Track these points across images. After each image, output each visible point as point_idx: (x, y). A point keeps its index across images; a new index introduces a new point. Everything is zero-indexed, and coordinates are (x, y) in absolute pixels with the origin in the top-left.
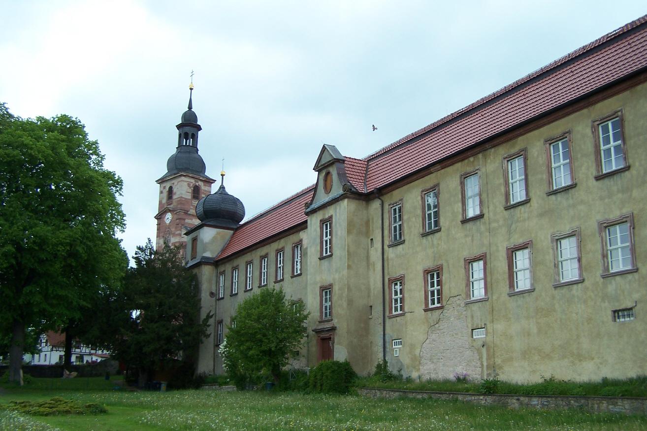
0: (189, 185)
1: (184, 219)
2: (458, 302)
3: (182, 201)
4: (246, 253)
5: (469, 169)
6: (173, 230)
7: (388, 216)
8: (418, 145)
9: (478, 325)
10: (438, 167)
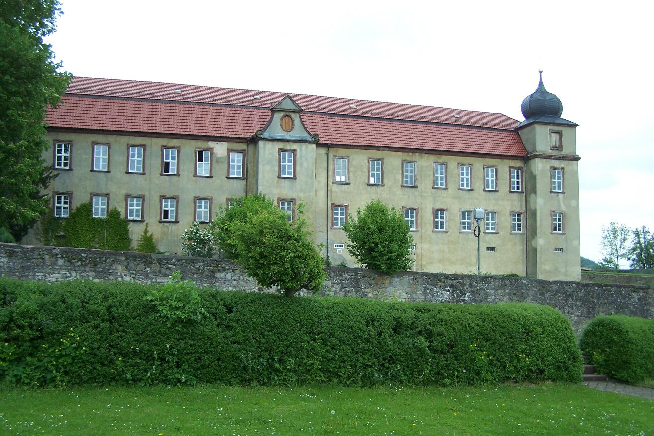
5: (408, 159)
10: (387, 149)
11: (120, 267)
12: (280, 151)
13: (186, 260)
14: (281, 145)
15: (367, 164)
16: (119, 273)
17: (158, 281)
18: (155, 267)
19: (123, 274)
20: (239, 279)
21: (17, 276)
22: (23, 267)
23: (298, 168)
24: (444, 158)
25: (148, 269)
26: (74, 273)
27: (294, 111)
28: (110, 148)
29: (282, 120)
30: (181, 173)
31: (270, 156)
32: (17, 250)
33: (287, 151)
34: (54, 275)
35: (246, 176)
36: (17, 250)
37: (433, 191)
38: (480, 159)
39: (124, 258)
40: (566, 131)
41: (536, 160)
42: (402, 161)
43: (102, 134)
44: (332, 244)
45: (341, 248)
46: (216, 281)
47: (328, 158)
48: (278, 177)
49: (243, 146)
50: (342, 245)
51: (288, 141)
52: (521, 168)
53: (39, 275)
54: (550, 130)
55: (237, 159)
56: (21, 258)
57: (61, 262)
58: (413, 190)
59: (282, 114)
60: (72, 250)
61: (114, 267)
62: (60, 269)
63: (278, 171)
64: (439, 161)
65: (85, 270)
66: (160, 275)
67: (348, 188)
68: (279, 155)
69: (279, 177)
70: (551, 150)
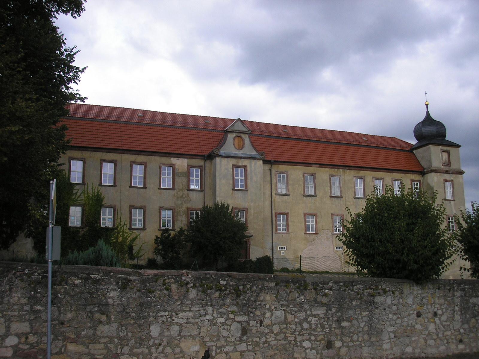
2: (327, 233)
4: (133, 154)
5: (334, 174)
8: (262, 140)
9: (339, 244)
10: (318, 166)
11: (268, 298)
12: (234, 167)
13: (344, 283)
14: (233, 161)
15: (302, 178)
16: (267, 306)
17: (314, 313)
18: (310, 294)
19: (273, 307)
20: (399, 302)
21: (133, 318)
22: (141, 305)
23: (249, 182)
24: (362, 173)
25: (302, 297)
26: (210, 310)
27: (244, 133)
28: (85, 163)
29: (235, 140)
30: (147, 185)
31: (226, 171)
32: (132, 278)
33: (239, 167)
34: (184, 314)
35: (203, 189)
36: (132, 278)
37: (355, 200)
38: (389, 173)
39: (273, 284)
40: (452, 150)
41: (433, 174)
42: (330, 175)
43: (78, 150)
44: (276, 247)
45: (340, 250)
46: (375, 308)
47: (271, 173)
48: (232, 189)
49: (200, 162)
50: (285, 248)
51: (240, 158)
52: (419, 181)
53: (162, 316)
54: (441, 149)
55: (195, 175)
56: (139, 291)
57: (193, 293)
58: (339, 199)
59: (234, 135)
60: (208, 276)
61: (262, 298)
62: (192, 304)
63: (232, 184)
64: (358, 175)
65: (225, 305)
66: (316, 305)
67: (288, 199)
68: (233, 170)
69: (233, 189)
70: (443, 165)
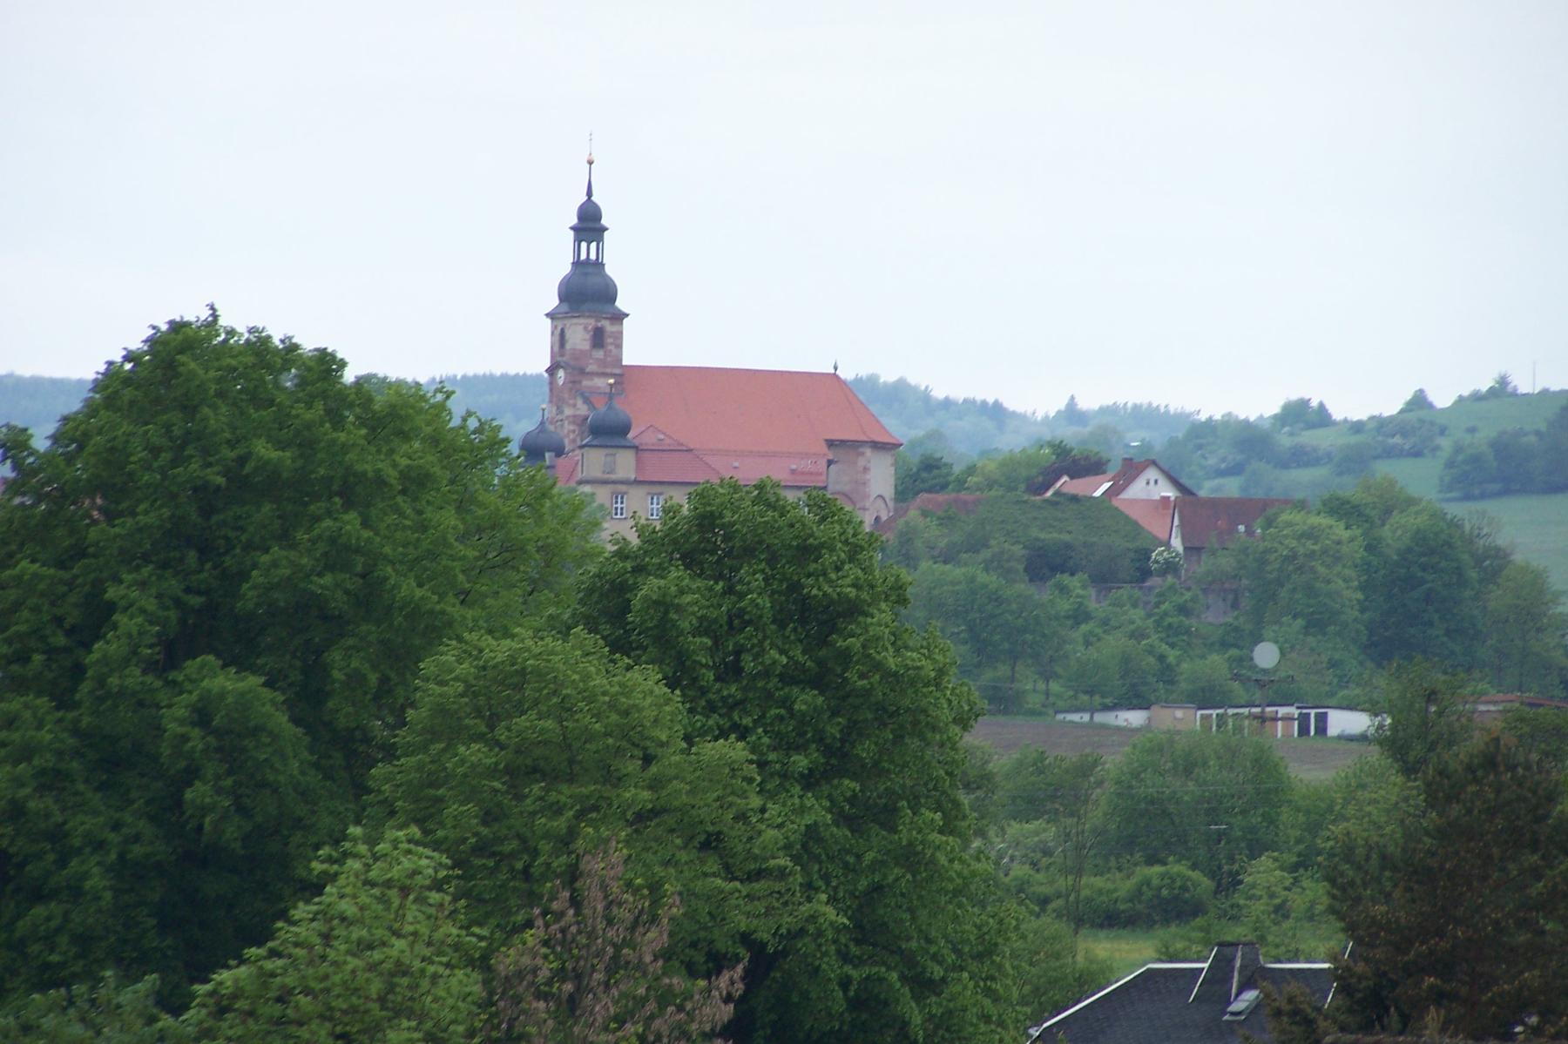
0: (585, 328)
1: (580, 382)
3: (579, 355)
6: (566, 396)
7: (20, 923)
